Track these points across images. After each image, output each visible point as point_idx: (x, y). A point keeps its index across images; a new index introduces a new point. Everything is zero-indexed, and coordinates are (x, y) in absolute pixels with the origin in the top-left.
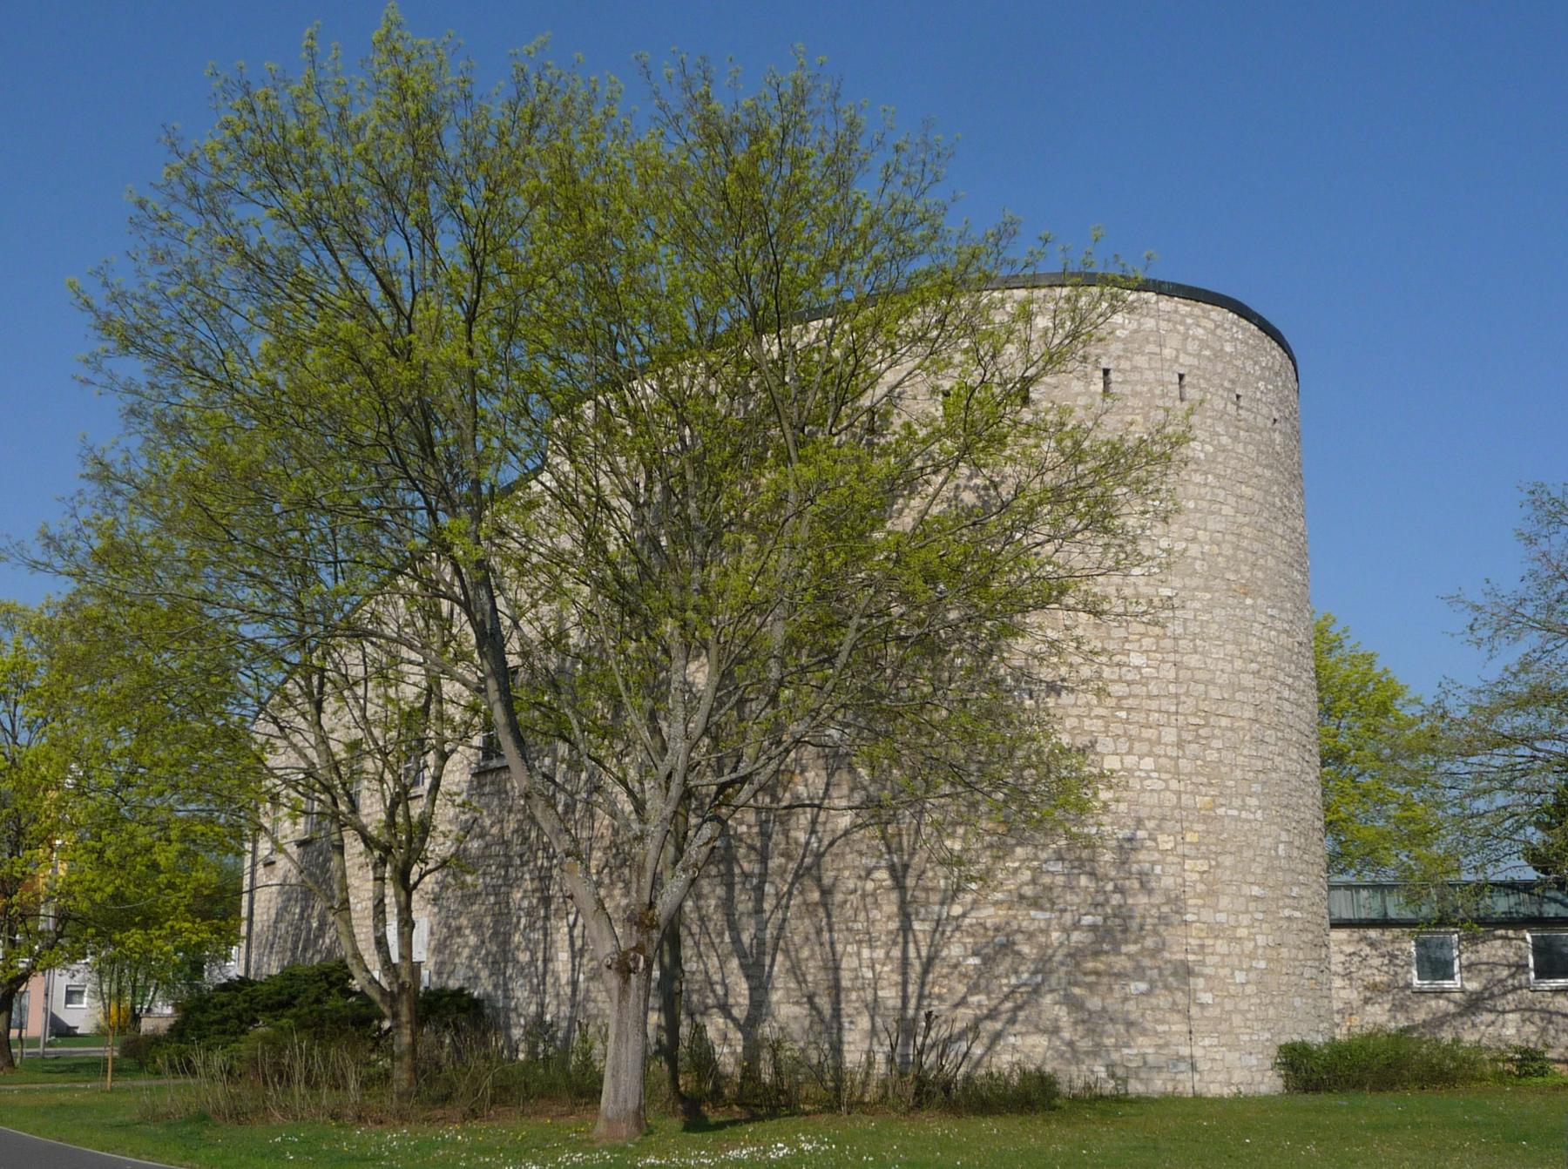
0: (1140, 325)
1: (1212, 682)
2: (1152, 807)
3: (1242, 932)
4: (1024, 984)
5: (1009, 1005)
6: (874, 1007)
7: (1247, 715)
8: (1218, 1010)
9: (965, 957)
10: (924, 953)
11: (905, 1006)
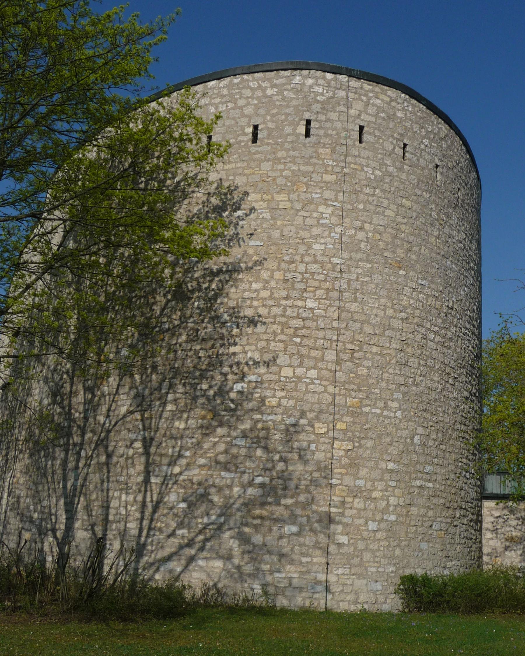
0: (334, 94)
1: (367, 322)
2: (313, 404)
3: (376, 494)
4: (213, 523)
5: (201, 537)
6: (123, 534)
7: (394, 346)
8: (352, 549)
9: (178, 502)
10: (155, 499)
11: (140, 535)
